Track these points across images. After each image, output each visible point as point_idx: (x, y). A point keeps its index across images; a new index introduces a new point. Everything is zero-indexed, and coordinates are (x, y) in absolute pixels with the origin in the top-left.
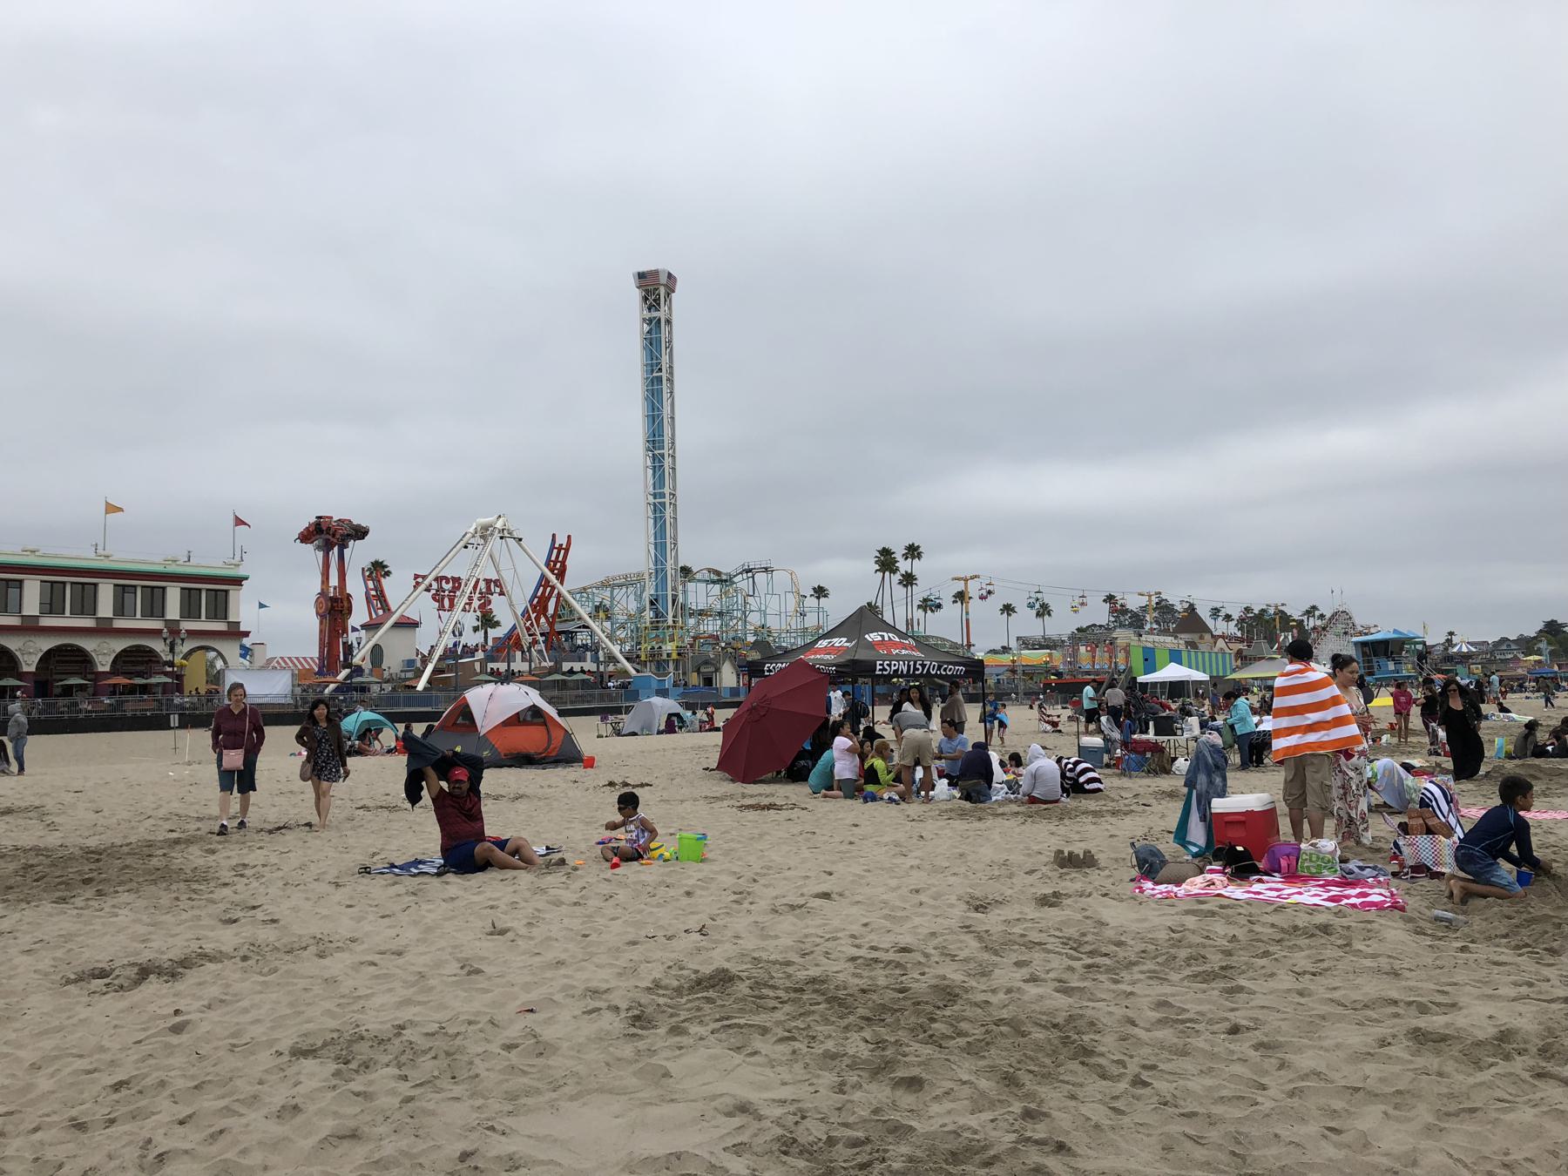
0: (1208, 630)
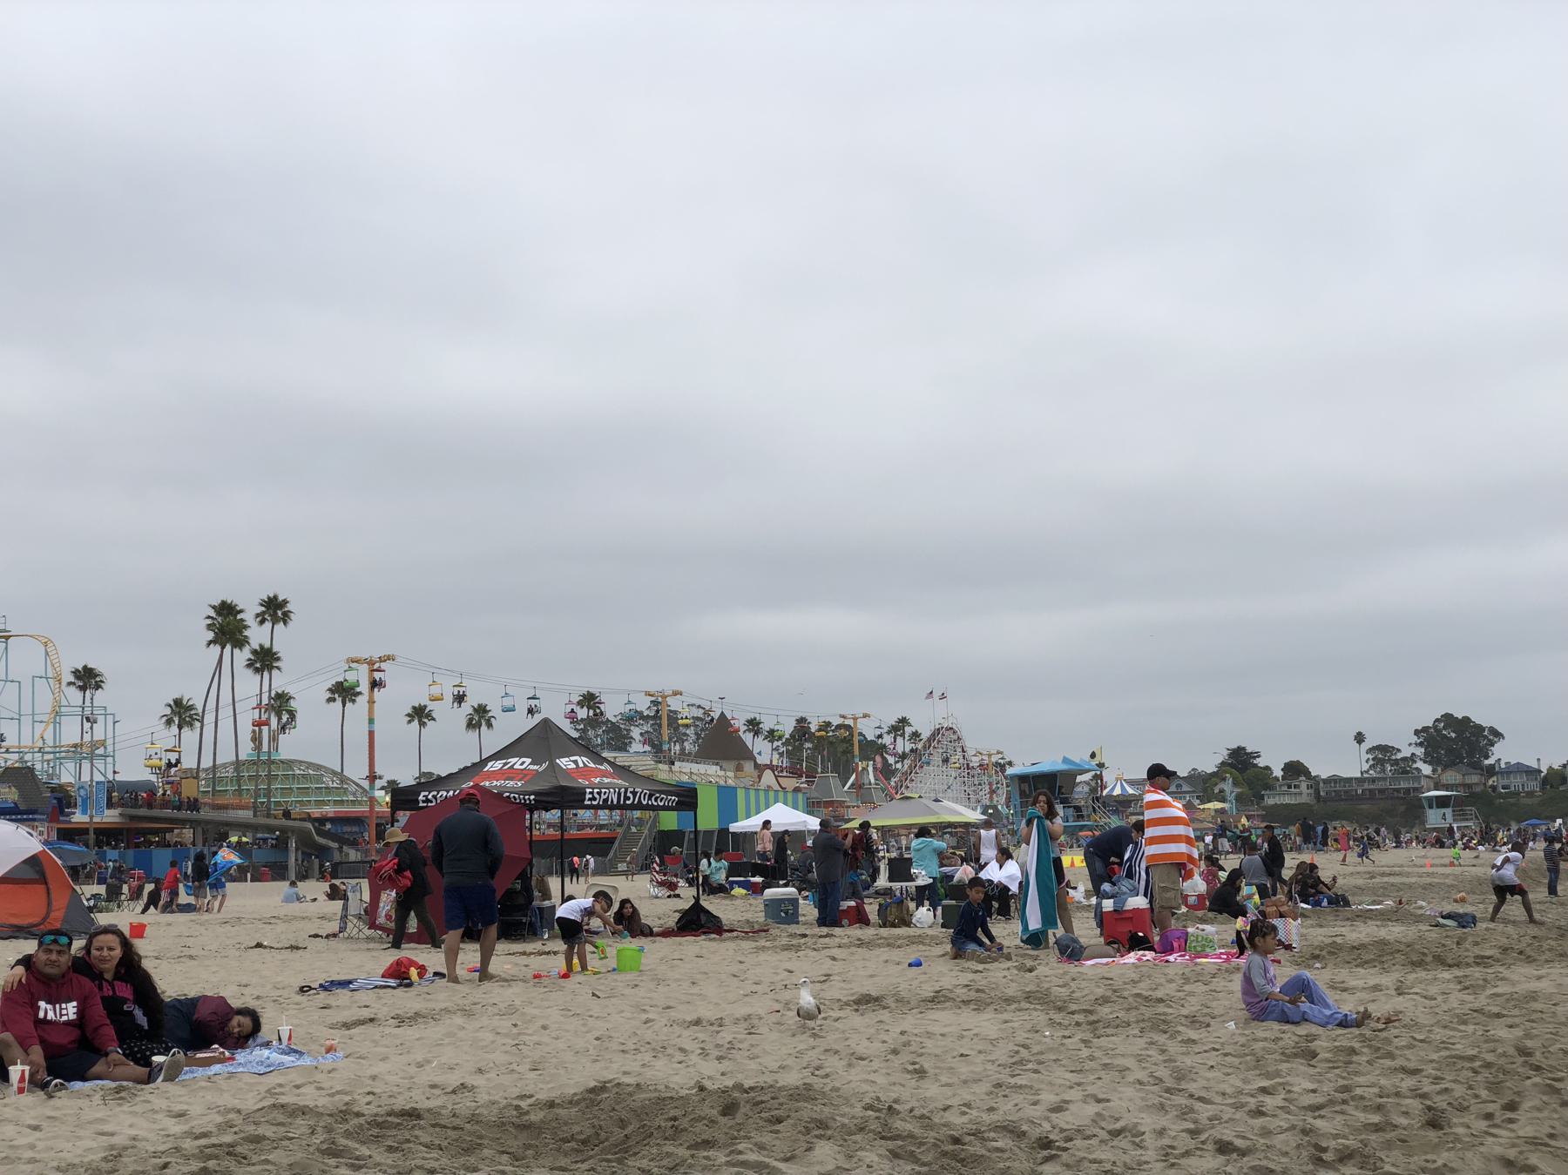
0: (749, 755)
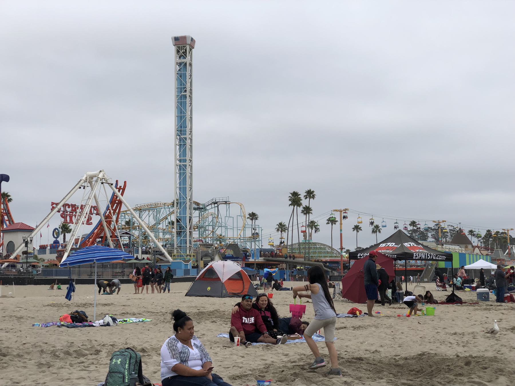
0: (470, 243)
